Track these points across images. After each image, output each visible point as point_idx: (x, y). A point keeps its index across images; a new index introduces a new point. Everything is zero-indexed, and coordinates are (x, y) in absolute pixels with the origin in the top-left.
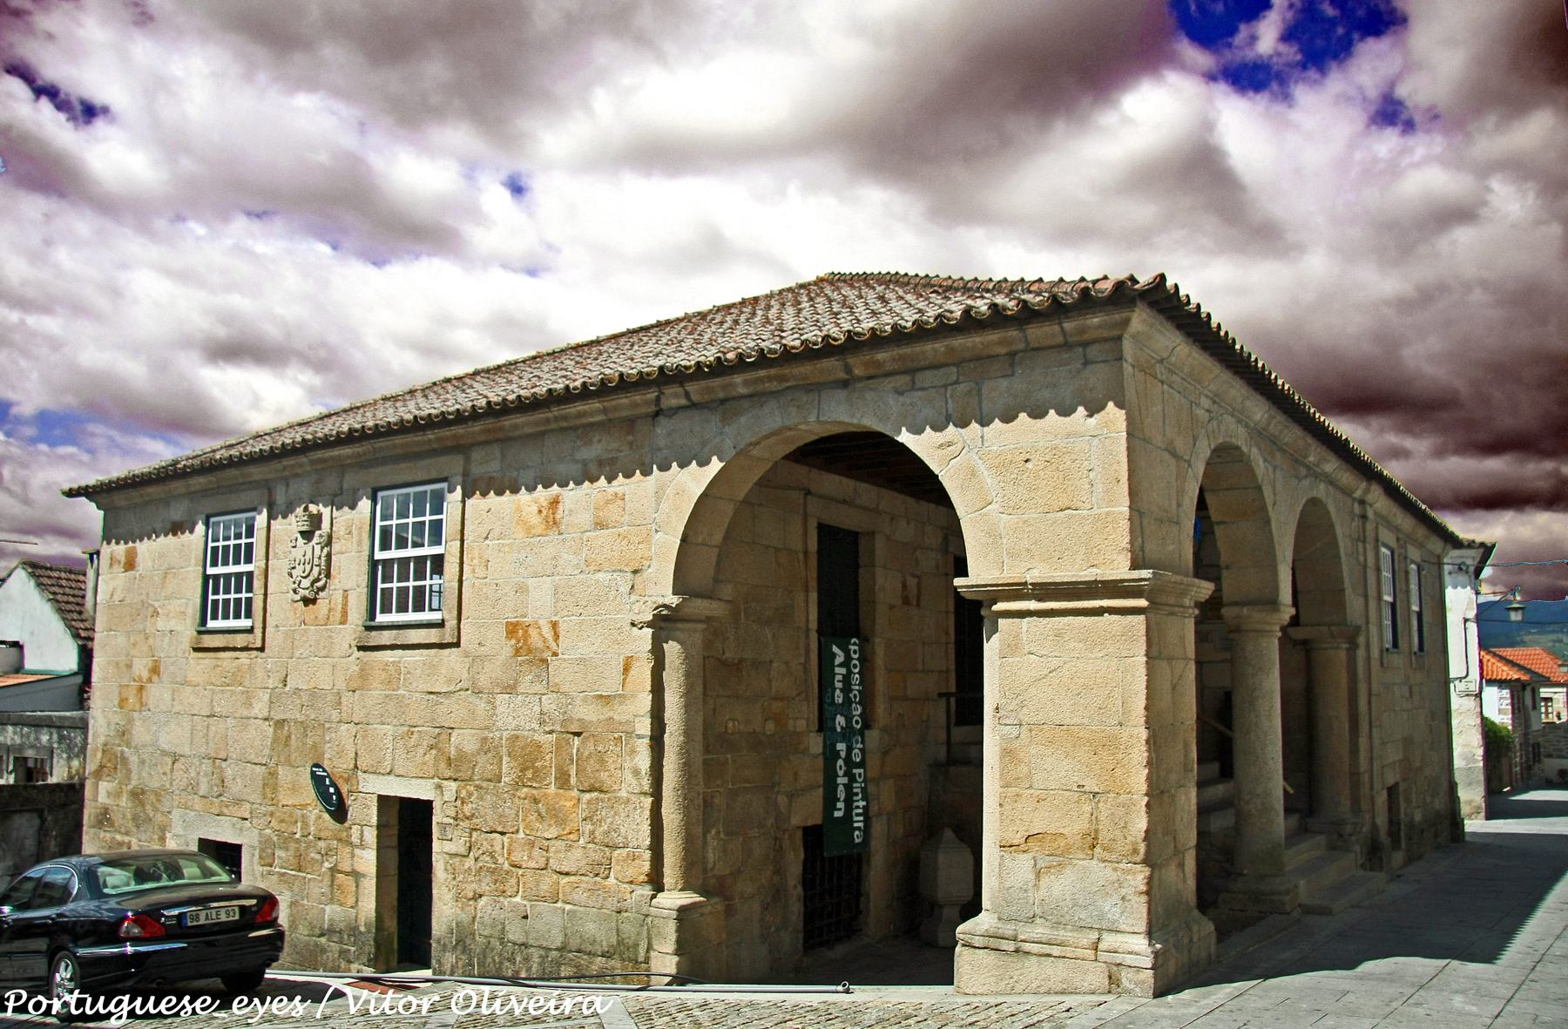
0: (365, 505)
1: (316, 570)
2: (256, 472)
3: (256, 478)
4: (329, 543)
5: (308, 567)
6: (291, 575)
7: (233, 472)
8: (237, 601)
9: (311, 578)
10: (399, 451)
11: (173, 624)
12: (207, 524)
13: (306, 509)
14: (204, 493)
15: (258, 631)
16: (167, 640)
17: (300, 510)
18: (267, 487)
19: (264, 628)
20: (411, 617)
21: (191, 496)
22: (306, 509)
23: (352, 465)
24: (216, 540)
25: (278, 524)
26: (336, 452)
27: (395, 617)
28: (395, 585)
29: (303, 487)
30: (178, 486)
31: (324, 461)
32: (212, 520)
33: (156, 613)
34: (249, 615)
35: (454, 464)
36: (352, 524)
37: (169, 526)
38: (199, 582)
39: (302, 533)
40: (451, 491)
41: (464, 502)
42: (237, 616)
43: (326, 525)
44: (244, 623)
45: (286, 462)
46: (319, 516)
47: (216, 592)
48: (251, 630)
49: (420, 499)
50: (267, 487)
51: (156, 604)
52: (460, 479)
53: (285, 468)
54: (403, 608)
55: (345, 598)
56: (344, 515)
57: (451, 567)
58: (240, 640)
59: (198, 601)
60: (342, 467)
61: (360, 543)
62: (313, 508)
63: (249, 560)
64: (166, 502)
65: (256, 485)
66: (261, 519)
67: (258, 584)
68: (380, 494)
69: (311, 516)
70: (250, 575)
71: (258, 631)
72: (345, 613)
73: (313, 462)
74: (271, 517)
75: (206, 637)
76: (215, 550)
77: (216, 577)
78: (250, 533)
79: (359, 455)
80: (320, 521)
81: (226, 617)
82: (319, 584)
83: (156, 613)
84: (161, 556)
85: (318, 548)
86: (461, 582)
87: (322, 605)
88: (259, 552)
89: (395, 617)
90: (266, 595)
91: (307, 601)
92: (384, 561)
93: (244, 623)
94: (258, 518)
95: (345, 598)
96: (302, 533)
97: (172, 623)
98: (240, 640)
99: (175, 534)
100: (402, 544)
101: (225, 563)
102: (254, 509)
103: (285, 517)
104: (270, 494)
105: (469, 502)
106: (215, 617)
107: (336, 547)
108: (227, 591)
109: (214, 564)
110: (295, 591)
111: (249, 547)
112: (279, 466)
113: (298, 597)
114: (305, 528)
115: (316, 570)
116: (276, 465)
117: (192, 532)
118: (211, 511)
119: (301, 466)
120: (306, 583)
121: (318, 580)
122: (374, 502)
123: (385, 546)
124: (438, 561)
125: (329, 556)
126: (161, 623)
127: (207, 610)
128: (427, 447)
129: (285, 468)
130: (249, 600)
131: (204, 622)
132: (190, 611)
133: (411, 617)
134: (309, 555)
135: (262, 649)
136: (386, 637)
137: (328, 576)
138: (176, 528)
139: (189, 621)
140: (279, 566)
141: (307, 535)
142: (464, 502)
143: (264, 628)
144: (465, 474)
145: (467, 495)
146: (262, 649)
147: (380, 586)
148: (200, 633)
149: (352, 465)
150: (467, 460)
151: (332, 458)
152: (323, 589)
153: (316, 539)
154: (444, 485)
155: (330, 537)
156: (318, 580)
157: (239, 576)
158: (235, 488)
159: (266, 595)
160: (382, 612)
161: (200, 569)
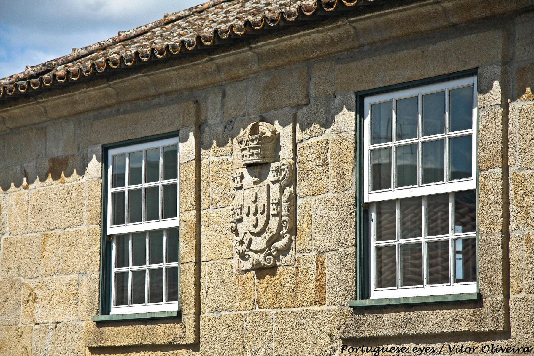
0: (346, 119)
1: (274, 222)
2: (174, 76)
3: (175, 86)
4: (292, 181)
5: (262, 219)
6: (235, 232)
7: (141, 78)
8: (156, 274)
9: (267, 235)
10: (396, 32)
11: (58, 313)
12: (104, 160)
13: (255, 130)
14: (98, 112)
15: (189, 319)
16: (50, 336)
17: (245, 133)
18: (194, 98)
19: (198, 314)
20: (428, 291)
21: (76, 116)
22: (255, 130)
23: (320, 59)
24: (119, 180)
25: (210, 156)
26: (297, 39)
27: (131, 310)
28: (130, 268)
29: (250, 96)
30: (56, 102)
31: (275, 54)
32: (112, 152)
33: (33, 297)
34: (173, 296)
35: (492, 42)
36: (328, 148)
37: (47, 165)
38: (97, 248)
39: (249, 166)
40: (484, 89)
41: (505, 106)
42: (156, 298)
43: (286, 153)
44: (169, 307)
45: (220, 59)
46: (276, 138)
47: (122, 262)
48: (178, 318)
49: (406, 108)
50: (194, 98)
51: (33, 283)
52: (498, 70)
53: (219, 68)
54: (412, 279)
55: (321, 264)
56: (315, 138)
57: (487, 213)
58: (162, 333)
59: (96, 275)
60: (307, 62)
61: (340, 179)
62: (265, 128)
63: (170, 213)
64: (41, 129)
65: (174, 96)
66: (186, 149)
67: (185, 247)
68: (368, 101)
69: (262, 140)
70: (173, 233)
71: (189, 319)
72: (321, 288)
73: (260, 58)
74: (200, 146)
75: (108, 330)
76: (118, 197)
77: (122, 239)
78: (171, 171)
79: (333, 42)
80: (277, 148)
81: (139, 300)
82: (280, 244)
83: (33, 297)
84: (39, 210)
85: (275, 189)
86: (506, 233)
87: (285, 273)
88: (185, 198)
89: (131, 310)
90: (198, 263)
91: (261, 271)
92: (379, 204)
93: (169, 307)
94: (182, 146)
95: (321, 264)
96: (249, 166)
97: (58, 311)
98: (162, 333)
99: (56, 177)
100: (407, 178)
101: (135, 218)
102: (175, 134)
103: (222, 144)
104: (198, 111)
105: (515, 106)
106: (121, 301)
107: (303, 186)
108: (139, 260)
109: (118, 220)
110: (243, 256)
111: (171, 190)
112: (211, 66)
113: (247, 265)
114: (254, 159)
115: (274, 222)
116: (204, 64)
117: (82, 172)
118: (362, 88)
119: (244, 63)
120: (259, 243)
121: (277, 238)
122: (360, 112)
123: (380, 182)
124: (467, 201)
125: (293, 198)
126: (41, 313)
127: (110, 290)
128: (442, 23)
129: (219, 68)
130: (173, 273)
131: (105, 309)
132: (84, 291)
133: (428, 291)
134: (262, 200)
135: (195, 346)
136: (388, 324)
137: (293, 231)
138: (58, 168)
139: (82, 308)
140: (216, 217)
141: (259, 169)
142: (505, 106)
143: (198, 314)
144: (506, 62)
145: (509, 96)
146: (195, 346)
147: (114, 270)
148: (100, 324)
149: (320, 59)
150: (509, 38)
151: (292, 50)
152: (286, 250)
153: (271, 177)
154: (473, 80)
155: (293, 170)
156: (277, 238)
157: (156, 234)
158: (146, 102)
159: (198, 263)
160: (379, 285)
161: (97, 228)
